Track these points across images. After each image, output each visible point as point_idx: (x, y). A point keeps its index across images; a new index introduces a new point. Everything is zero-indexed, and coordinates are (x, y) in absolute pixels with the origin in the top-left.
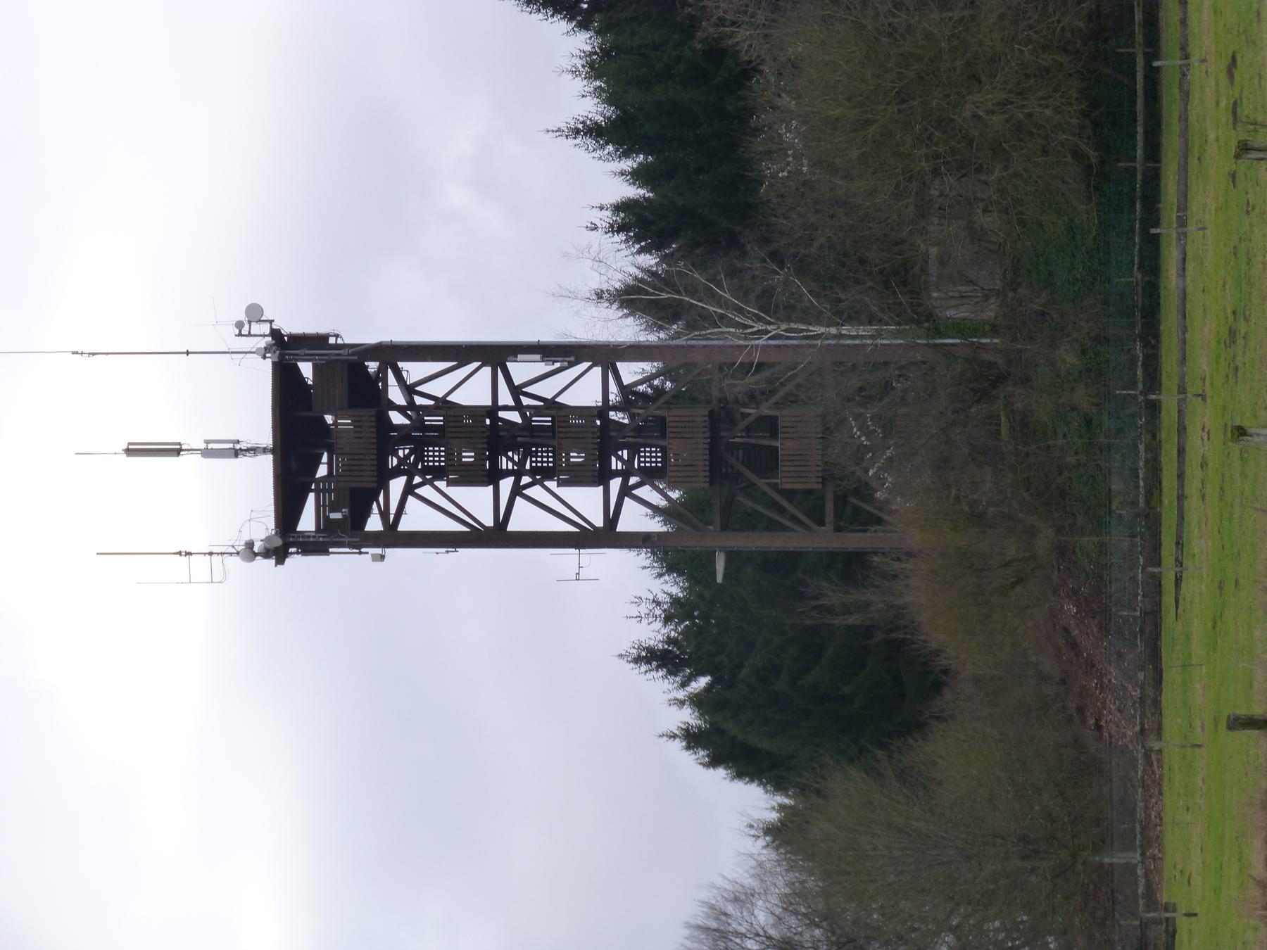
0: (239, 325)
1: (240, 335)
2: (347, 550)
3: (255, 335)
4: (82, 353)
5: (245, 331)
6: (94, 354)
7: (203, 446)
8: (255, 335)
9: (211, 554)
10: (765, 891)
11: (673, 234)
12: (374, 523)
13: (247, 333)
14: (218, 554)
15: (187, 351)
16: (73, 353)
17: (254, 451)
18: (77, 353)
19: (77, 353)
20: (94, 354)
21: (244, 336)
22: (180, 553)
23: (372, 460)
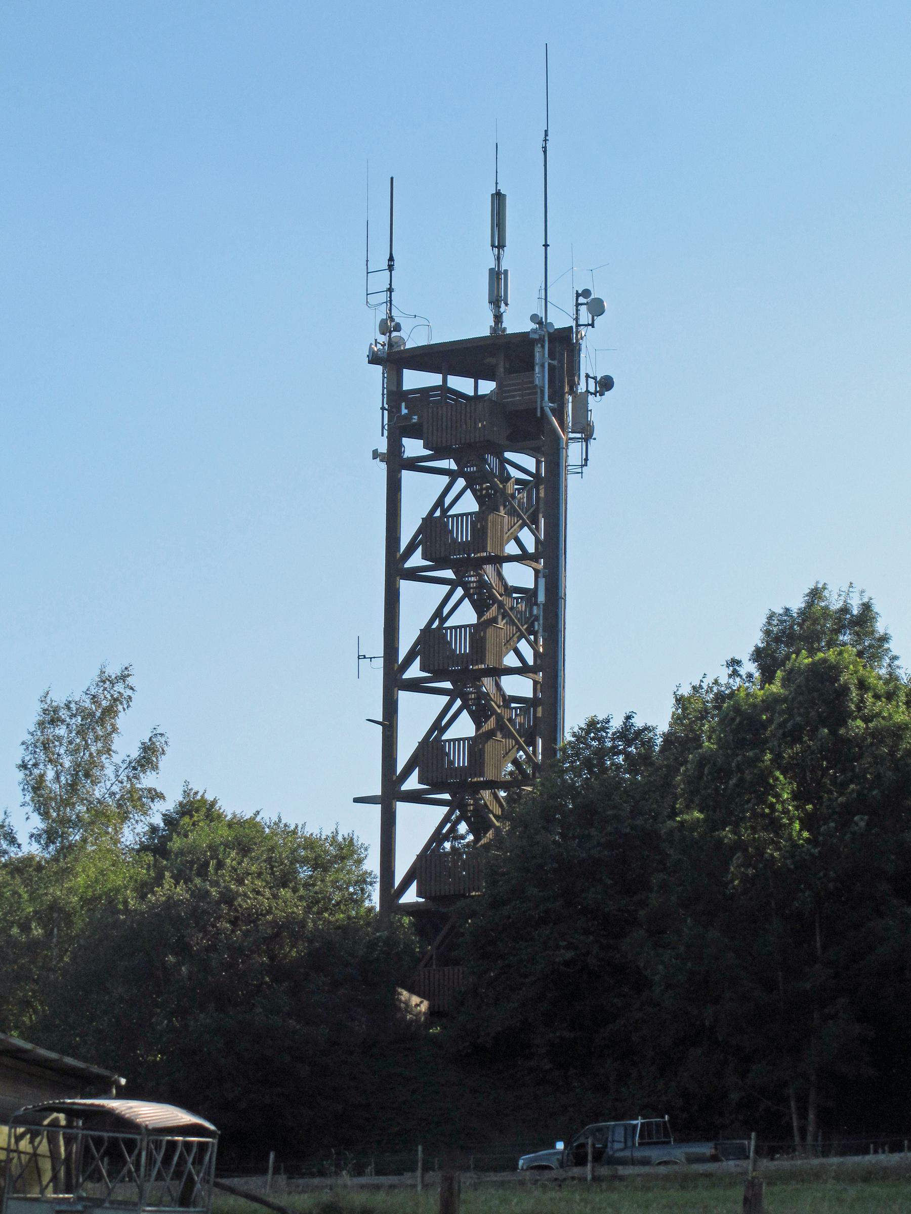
0: (586, 293)
1: (578, 295)
2: (386, 421)
3: (577, 310)
4: (546, 140)
5: (581, 300)
6: (545, 152)
7: (503, 268)
8: (577, 310)
9: (390, 290)
10: (9, 911)
11: (472, 917)
12: (413, 447)
13: (579, 302)
14: (390, 297)
15: (544, 245)
16: (546, 131)
17: (498, 318)
18: (546, 135)
19: (546, 135)
20: (545, 152)
21: (577, 300)
22: (391, 259)
23: (475, 437)
